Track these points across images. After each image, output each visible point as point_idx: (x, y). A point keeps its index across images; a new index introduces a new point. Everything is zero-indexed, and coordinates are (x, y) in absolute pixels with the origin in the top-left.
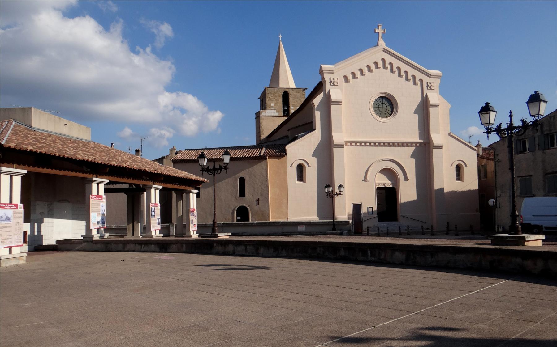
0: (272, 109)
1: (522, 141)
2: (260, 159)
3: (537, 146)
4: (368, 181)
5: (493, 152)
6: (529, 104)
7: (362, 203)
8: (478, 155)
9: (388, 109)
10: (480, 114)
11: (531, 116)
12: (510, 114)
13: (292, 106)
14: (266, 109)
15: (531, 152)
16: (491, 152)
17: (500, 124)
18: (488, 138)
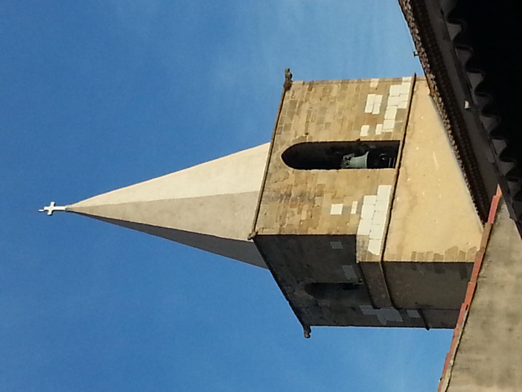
0: (359, 212)
13: (356, 132)
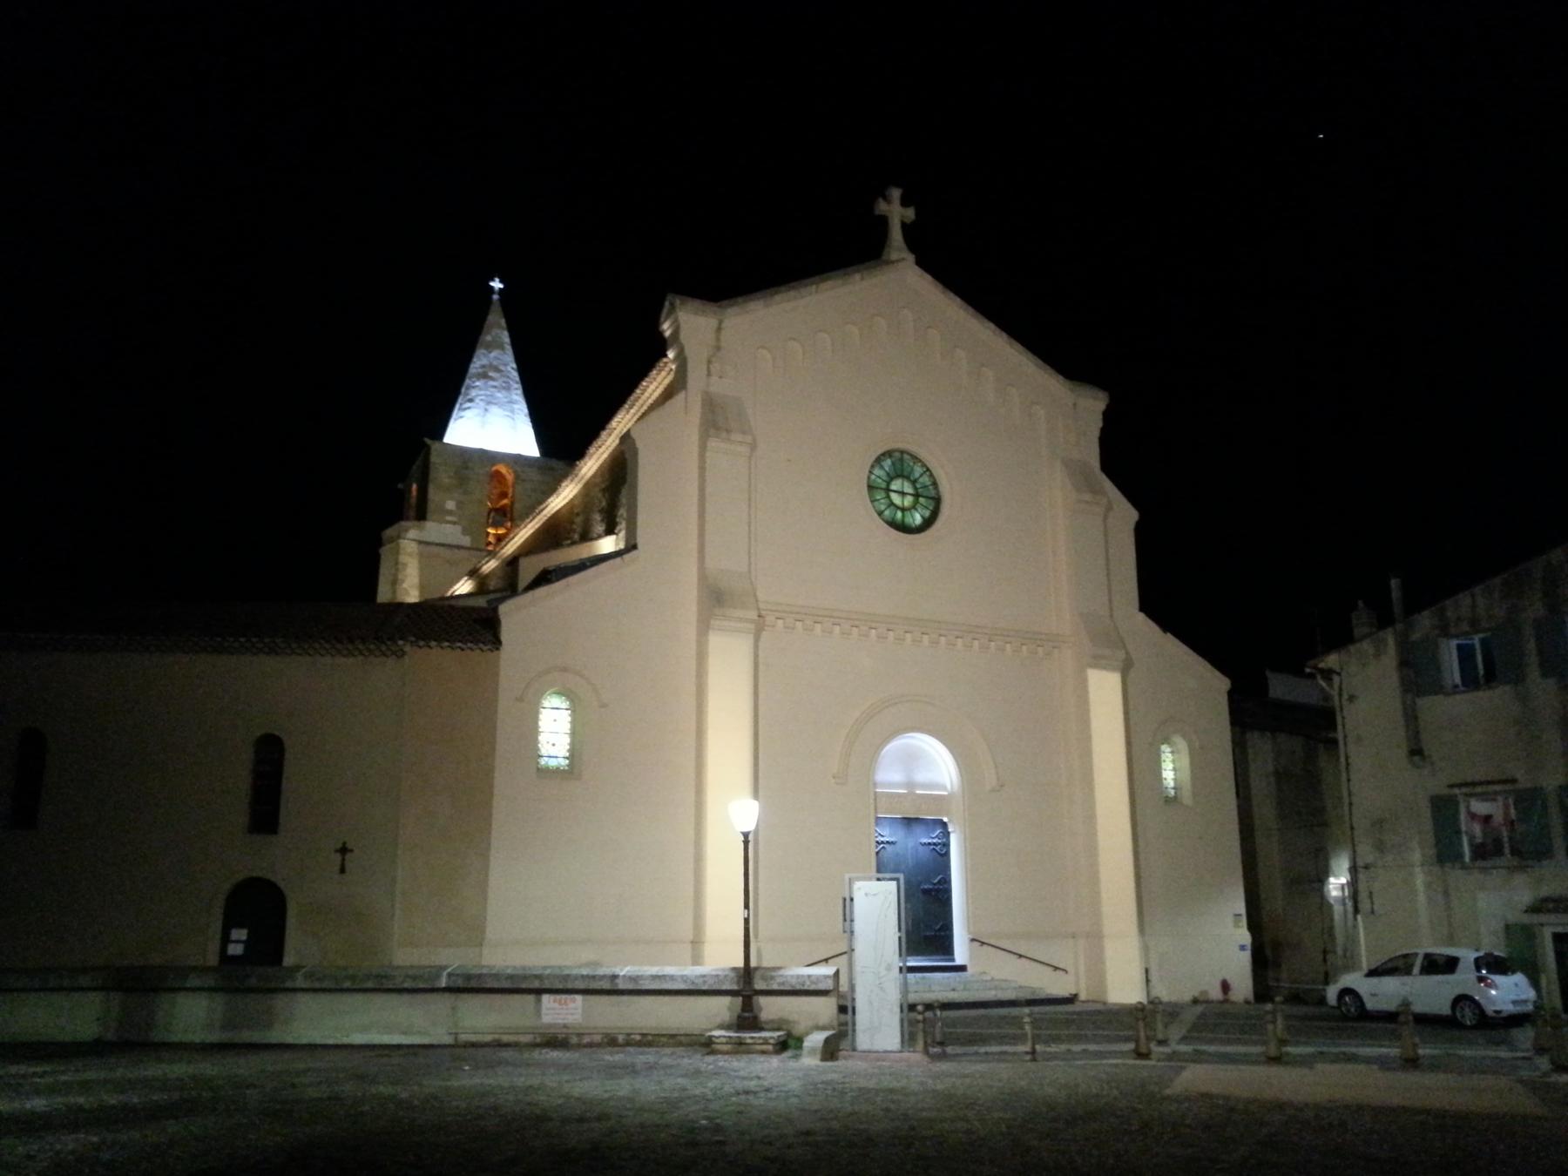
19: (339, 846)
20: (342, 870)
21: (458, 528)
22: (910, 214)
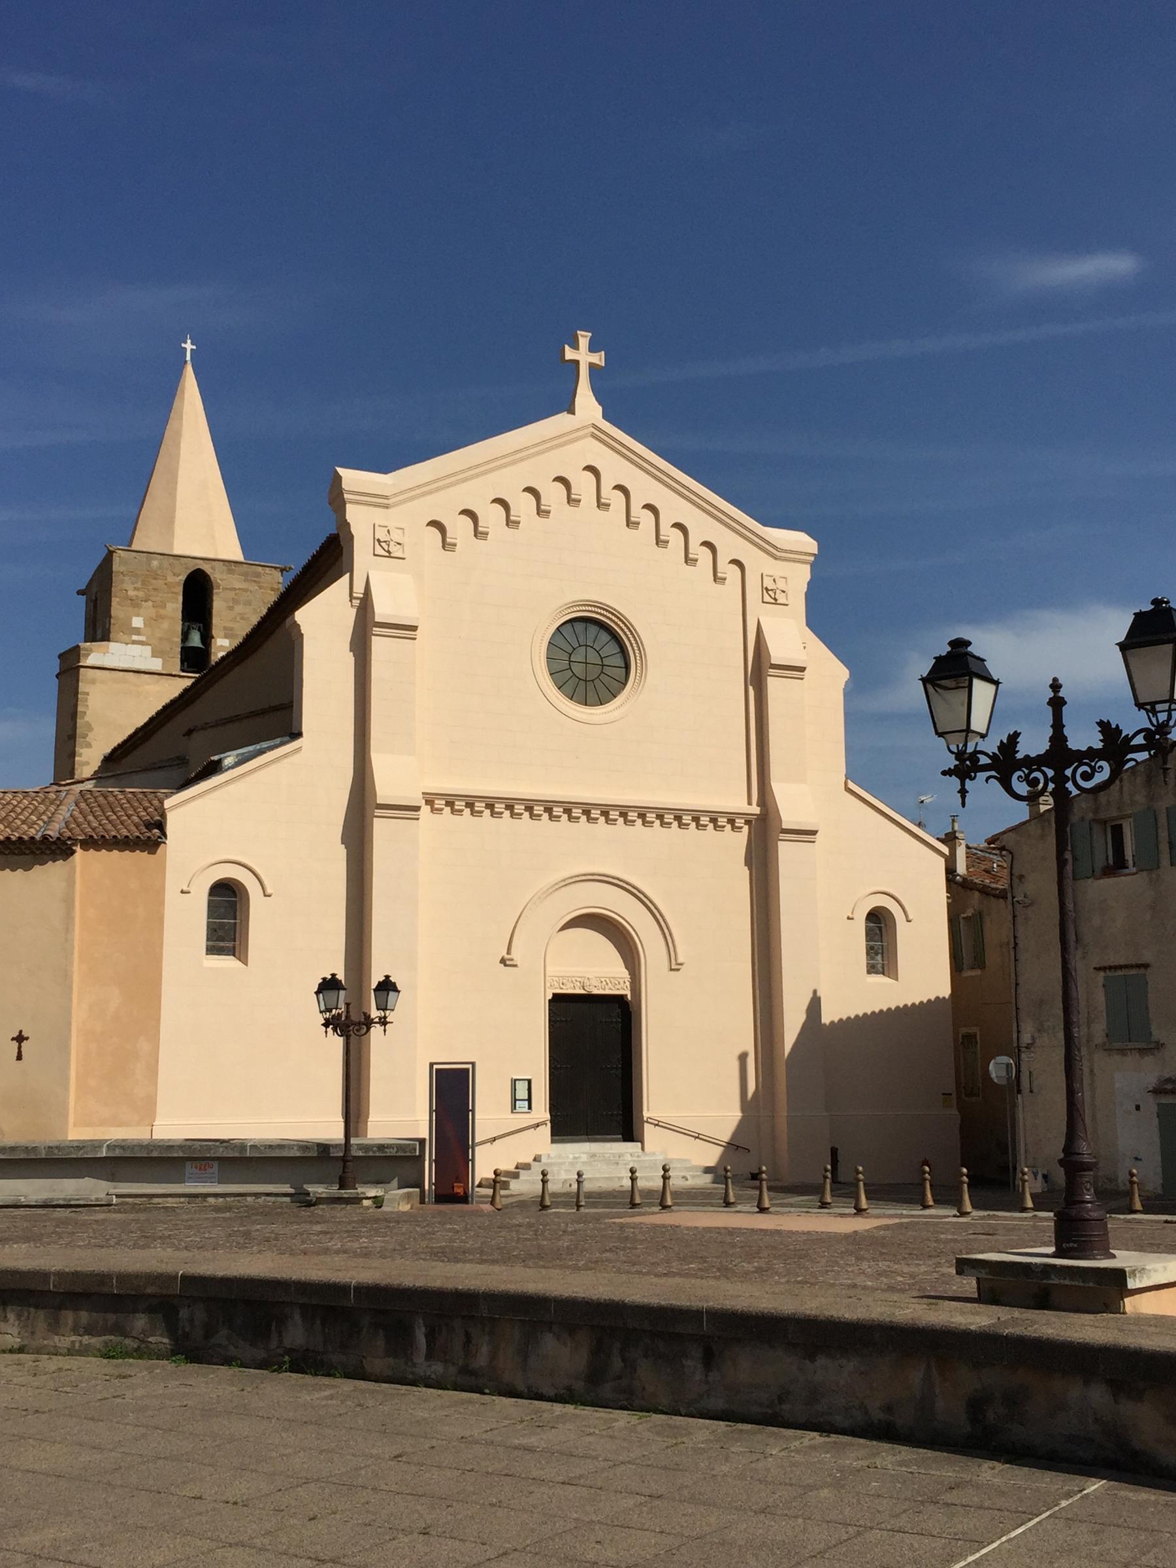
0: (134, 642)
1: (1112, 827)
2: (43, 853)
3: (1164, 847)
4: (515, 966)
5: (1005, 866)
6: (1128, 653)
7: (473, 1064)
8: (950, 871)
9: (607, 670)
10: (929, 687)
11: (1140, 706)
12: (1052, 695)
13: (222, 634)
14: (106, 638)
15: (1142, 871)
16: (998, 866)
17: (1014, 738)
18: (963, 798)
19: (16, 1034)
20: (19, 1057)
21: (148, 650)
22: (598, 359)
